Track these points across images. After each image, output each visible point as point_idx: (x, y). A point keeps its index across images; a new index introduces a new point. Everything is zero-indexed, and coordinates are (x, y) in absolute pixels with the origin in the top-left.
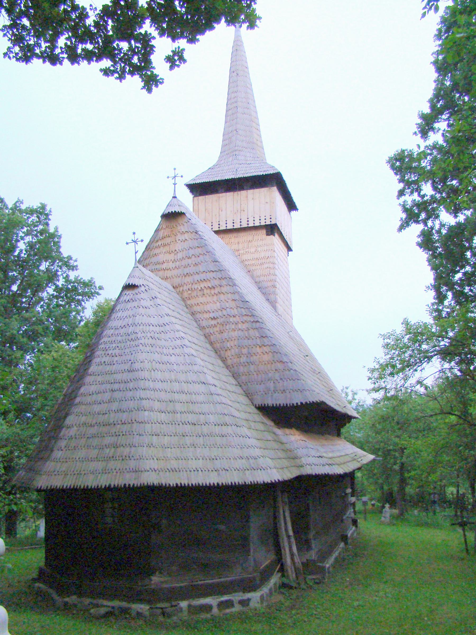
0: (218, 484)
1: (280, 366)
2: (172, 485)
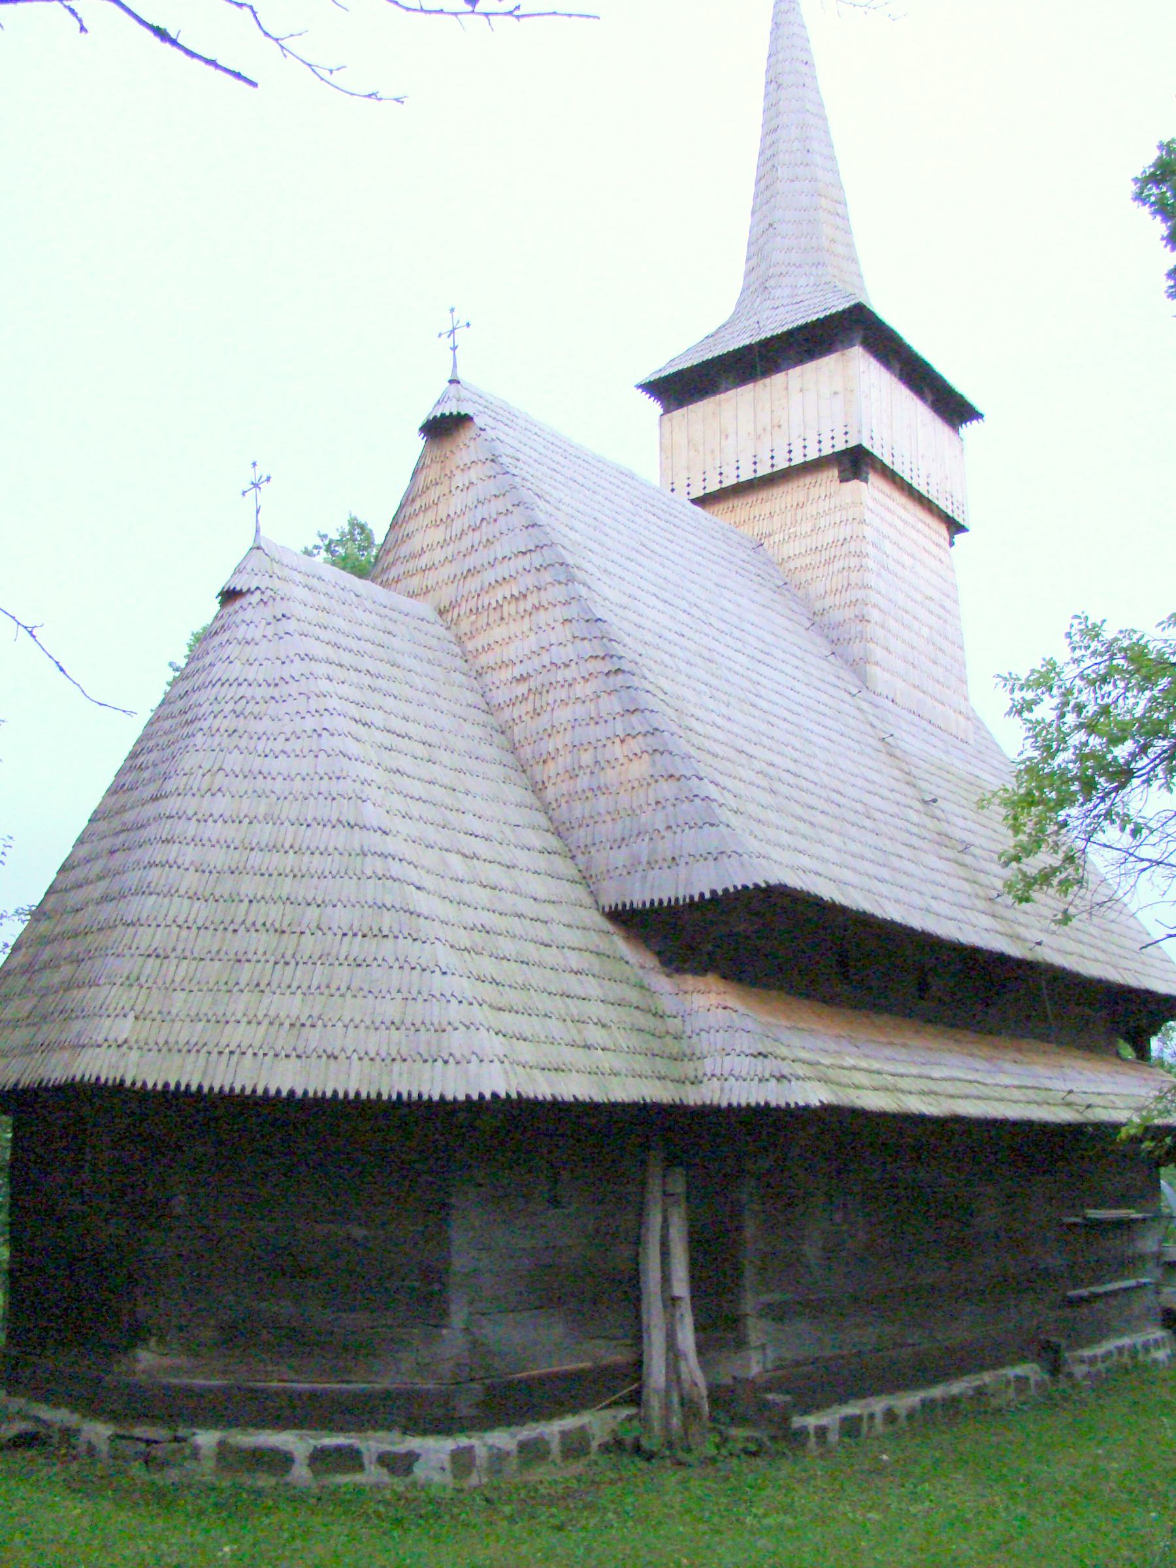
0: (292, 1093)
1: (667, 789)
2: (150, 1086)
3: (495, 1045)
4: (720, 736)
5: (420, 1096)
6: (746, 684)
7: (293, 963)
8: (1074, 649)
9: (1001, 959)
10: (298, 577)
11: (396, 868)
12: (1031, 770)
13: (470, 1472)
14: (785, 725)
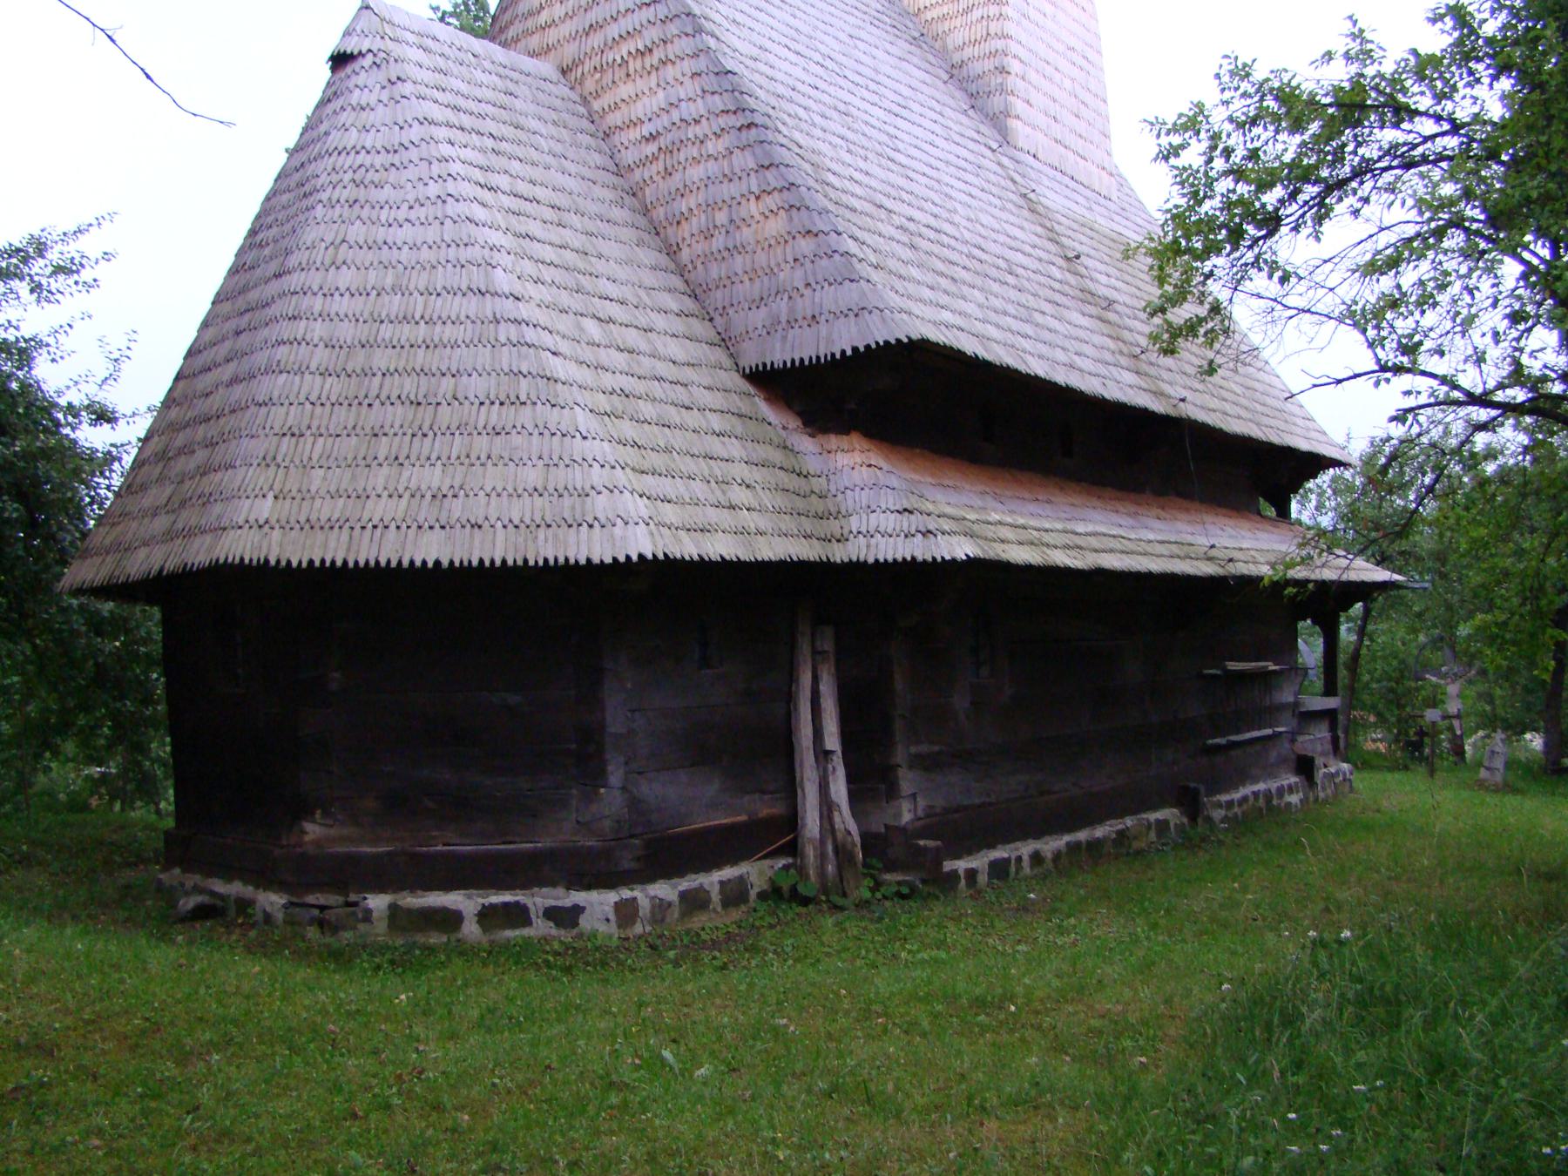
0: (437, 563)
1: (805, 246)
2: (295, 564)
3: (641, 507)
4: (859, 191)
5: (567, 559)
6: (884, 138)
7: (431, 434)
8: (1223, 90)
9: (1144, 414)
10: (411, 38)
11: (530, 335)
12: (1178, 218)
13: (634, 923)
14: (924, 180)
